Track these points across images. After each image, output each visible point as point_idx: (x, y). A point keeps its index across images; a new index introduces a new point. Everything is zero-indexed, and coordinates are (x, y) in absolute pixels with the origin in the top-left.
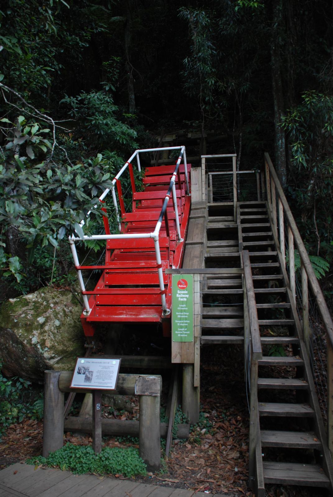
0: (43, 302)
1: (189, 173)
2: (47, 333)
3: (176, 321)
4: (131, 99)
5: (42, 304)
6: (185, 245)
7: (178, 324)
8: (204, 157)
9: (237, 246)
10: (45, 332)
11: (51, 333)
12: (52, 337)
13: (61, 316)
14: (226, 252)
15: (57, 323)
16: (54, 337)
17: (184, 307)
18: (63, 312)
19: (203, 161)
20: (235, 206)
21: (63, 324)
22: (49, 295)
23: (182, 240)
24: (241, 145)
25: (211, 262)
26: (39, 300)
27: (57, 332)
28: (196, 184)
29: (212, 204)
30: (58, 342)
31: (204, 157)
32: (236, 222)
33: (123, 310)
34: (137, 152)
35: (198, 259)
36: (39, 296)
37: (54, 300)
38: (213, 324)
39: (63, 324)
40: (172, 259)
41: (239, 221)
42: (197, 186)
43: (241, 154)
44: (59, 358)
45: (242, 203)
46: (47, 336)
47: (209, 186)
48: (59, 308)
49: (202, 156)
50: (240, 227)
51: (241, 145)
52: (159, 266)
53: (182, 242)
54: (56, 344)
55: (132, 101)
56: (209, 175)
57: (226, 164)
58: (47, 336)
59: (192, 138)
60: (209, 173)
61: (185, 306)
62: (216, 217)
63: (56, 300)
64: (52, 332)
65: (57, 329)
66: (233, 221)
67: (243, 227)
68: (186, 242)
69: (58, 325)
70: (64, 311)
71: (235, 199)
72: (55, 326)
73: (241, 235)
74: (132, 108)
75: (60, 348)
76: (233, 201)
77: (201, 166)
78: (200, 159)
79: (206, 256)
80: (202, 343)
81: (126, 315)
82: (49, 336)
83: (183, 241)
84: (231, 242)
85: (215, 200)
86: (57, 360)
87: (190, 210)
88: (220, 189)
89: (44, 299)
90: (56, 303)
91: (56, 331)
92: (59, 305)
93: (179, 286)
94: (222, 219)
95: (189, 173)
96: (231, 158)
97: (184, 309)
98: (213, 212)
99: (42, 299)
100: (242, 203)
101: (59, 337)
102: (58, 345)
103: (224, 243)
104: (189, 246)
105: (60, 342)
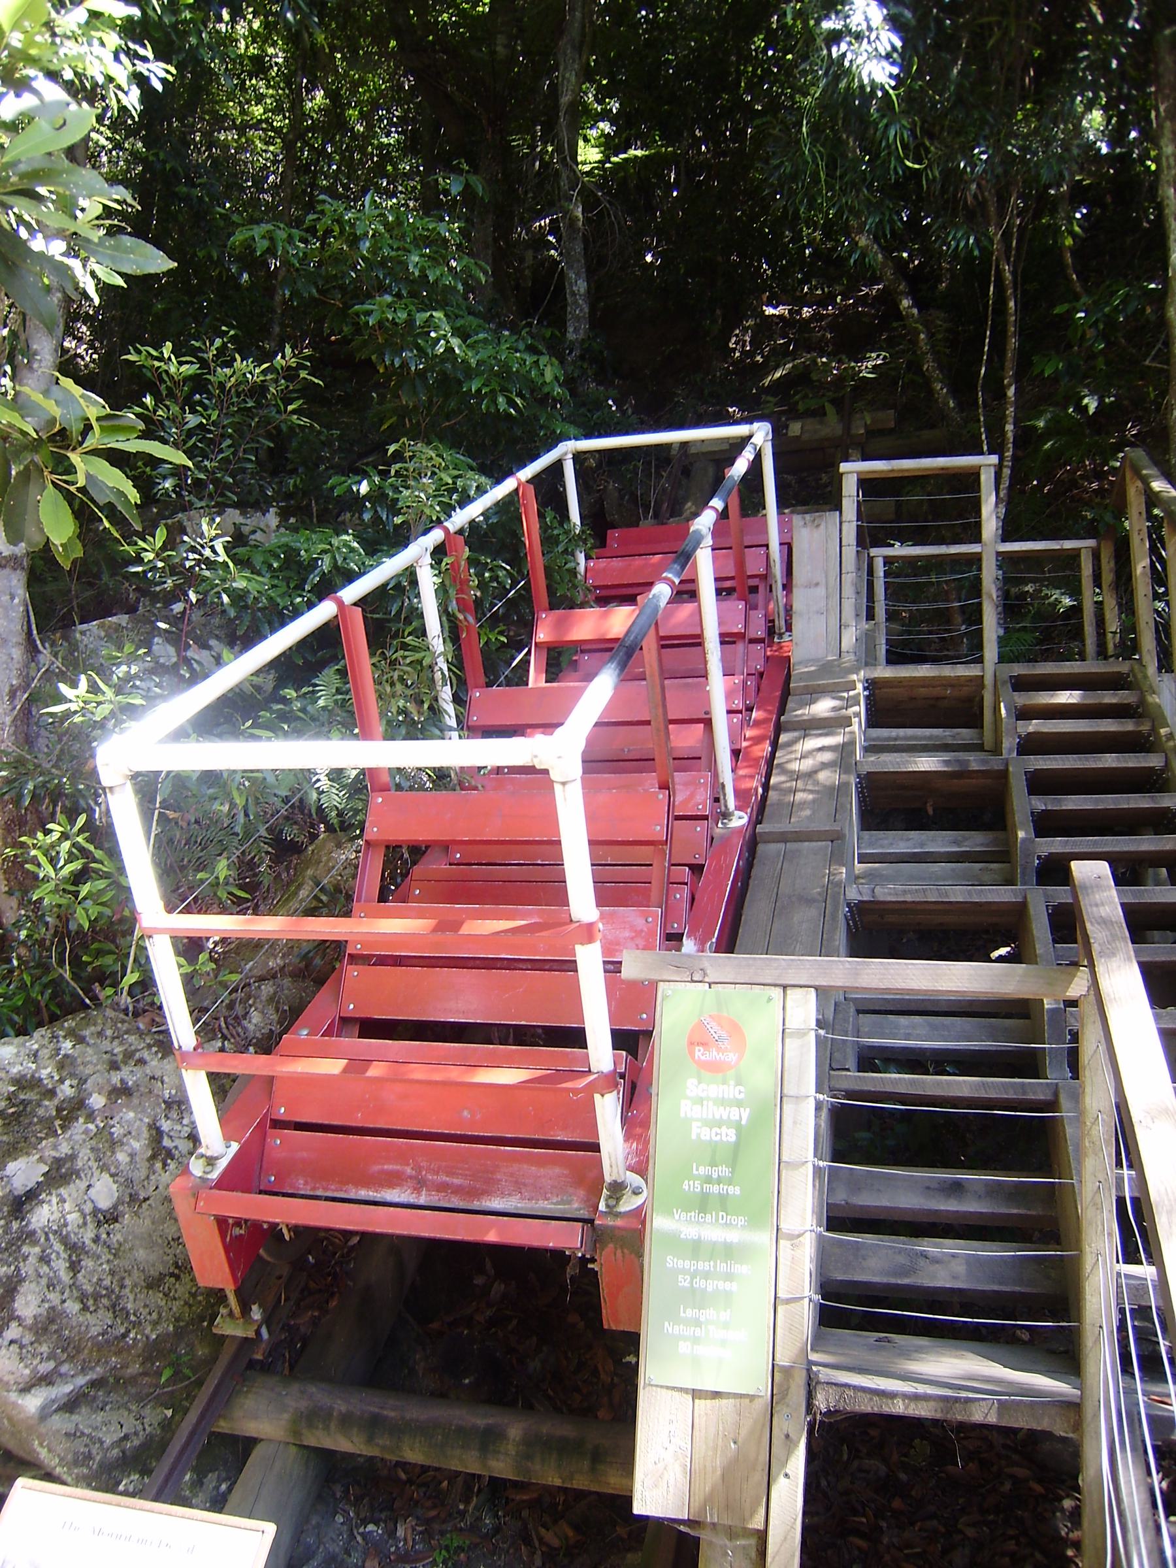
0: (62, 1081)
1: (788, 547)
2: (35, 1243)
3: (671, 1261)
4: (573, 294)
5: (52, 1093)
6: (752, 843)
7: (684, 1282)
8: (852, 470)
9: (1003, 855)
10: (29, 1236)
11: (58, 1247)
12: (61, 1266)
13: (132, 1155)
14: (955, 889)
15: (104, 1192)
16: (74, 1267)
17: (719, 1181)
18: (145, 1134)
19: (850, 487)
20: (988, 680)
21: (133, 1198)
22: (90, 1057)
23: (739, 820)
24: (1010, 435)
25: (879, 931)
26: (44, 1073)
27: (96, 1240)
28: (817, 584)
29: (885, 672)
30: (82, 1298)
31: (852, 470)
32: (997, 750)
33: (402, 1157)
34: (566, 449)
35: (813, 912)
36: (45, 1053)
37: (116, 1078)
38: (878, 1260)
39: (133, 1198)
40: (685, 905)
41: (1009, 744)
42: (821, 591)
43: (1011, 477)
44: (81, 1380)
45: (1019, 669)
46: (32, 1260)
47: (870, 616)
48: (129, 1116)
49: (844, 467)
50: (1020, 767)
51: (1010, 435)
52: (587, 933)
53: (738, 830)
54: (73, 1307)
55: (576, 302)
56: (871, 560)
57: (954, 505)
58: (32, 1260)
59: (806, 437)
60: (874, 552)
61: (724, 1171)
62: (902, 732)
63: (128, 1075)
64: (65, 1241)
65: (99, 1224)
66: (980, 748)
67: (1031, 768)
68: (759, 828)
69: (104, 1204)
70: (157, 1134)
71: (991, 652)
72: (88, 1208)
73: (1023, 805)
74: (576, 330)
75: (97, 1323)
76: (980, 660)
77: (838, 507)
78: (837, 480)
79: (853, 894)
80: (822, 1402)
81: (417, 1190)
82: (44, 1259)
83: (745, 820)
84: (975, 841)
85: (894, 658)
86: (68, 1388)
87: (786, 693)
88: (920, 615)
89: (65, 1064)
90: (122, 1092)
91: (88, 1235)
92: (136, 1101)
93: (699, 1052)
94: (930, 738)
95: (788, 547)
96: (971, 478)
97: (724, 1188)
98: (885, 708)
99: (61, 1066)
100: (1019, 669)
101: (94, 1270)
102: (85, 1308)
103: (938, 841)
104: (773, 847)
105: (97, 1297)
